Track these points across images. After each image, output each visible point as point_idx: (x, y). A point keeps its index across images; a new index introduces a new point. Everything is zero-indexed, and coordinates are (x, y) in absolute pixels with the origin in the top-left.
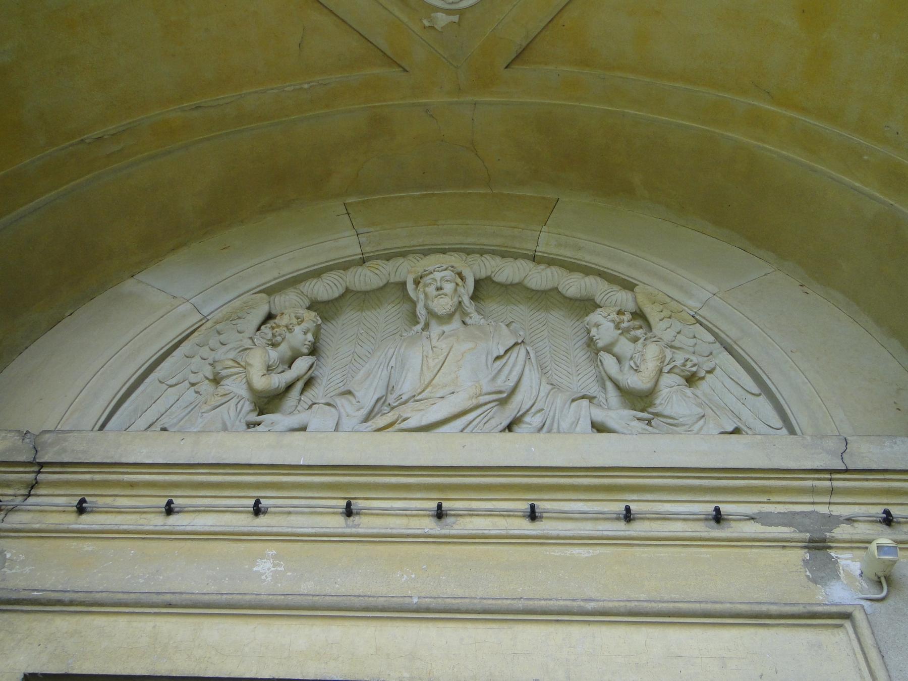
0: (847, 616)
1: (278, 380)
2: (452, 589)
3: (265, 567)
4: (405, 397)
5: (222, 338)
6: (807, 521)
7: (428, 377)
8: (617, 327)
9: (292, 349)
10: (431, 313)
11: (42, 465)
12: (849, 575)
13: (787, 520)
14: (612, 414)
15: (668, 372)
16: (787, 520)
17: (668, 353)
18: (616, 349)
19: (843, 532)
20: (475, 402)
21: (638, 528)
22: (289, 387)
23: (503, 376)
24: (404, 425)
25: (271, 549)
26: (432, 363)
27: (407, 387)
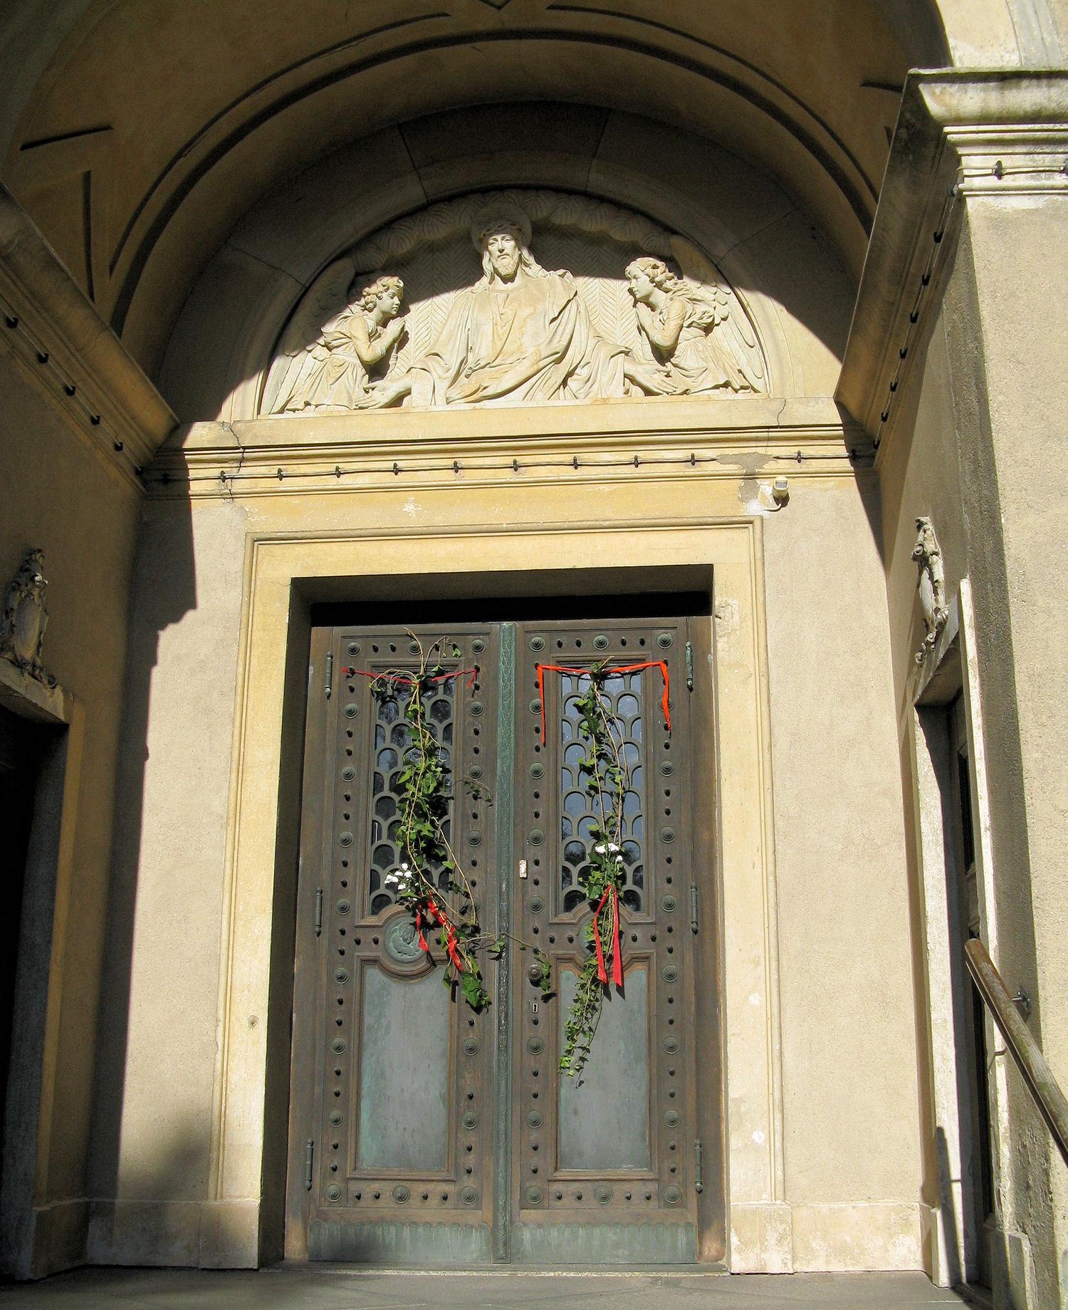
0: (751, 522)
1: (379, 347)
2: (527, 517)
3: (409, 508)
4: (483, 364)
5: (587, 780)
6: (749, 460)
7: (500, 344)
8: (652, 281)
9: (384, 313)
10: (496, 271)
11: (244, 448)
12: (764, 495)
13: (735, 460)
14: (640, 368)
15: (689, 326)
16: (735, 460)
17: (689, 307)
18: (651, 299)
19: (770, 466)
20: (536, 368)
21: (1007, 181)
22: (389, 350)
23: (557, 338)
24: (485, 393)
25: (412, 496)
26: (501, 332)
27: (484, 351)
